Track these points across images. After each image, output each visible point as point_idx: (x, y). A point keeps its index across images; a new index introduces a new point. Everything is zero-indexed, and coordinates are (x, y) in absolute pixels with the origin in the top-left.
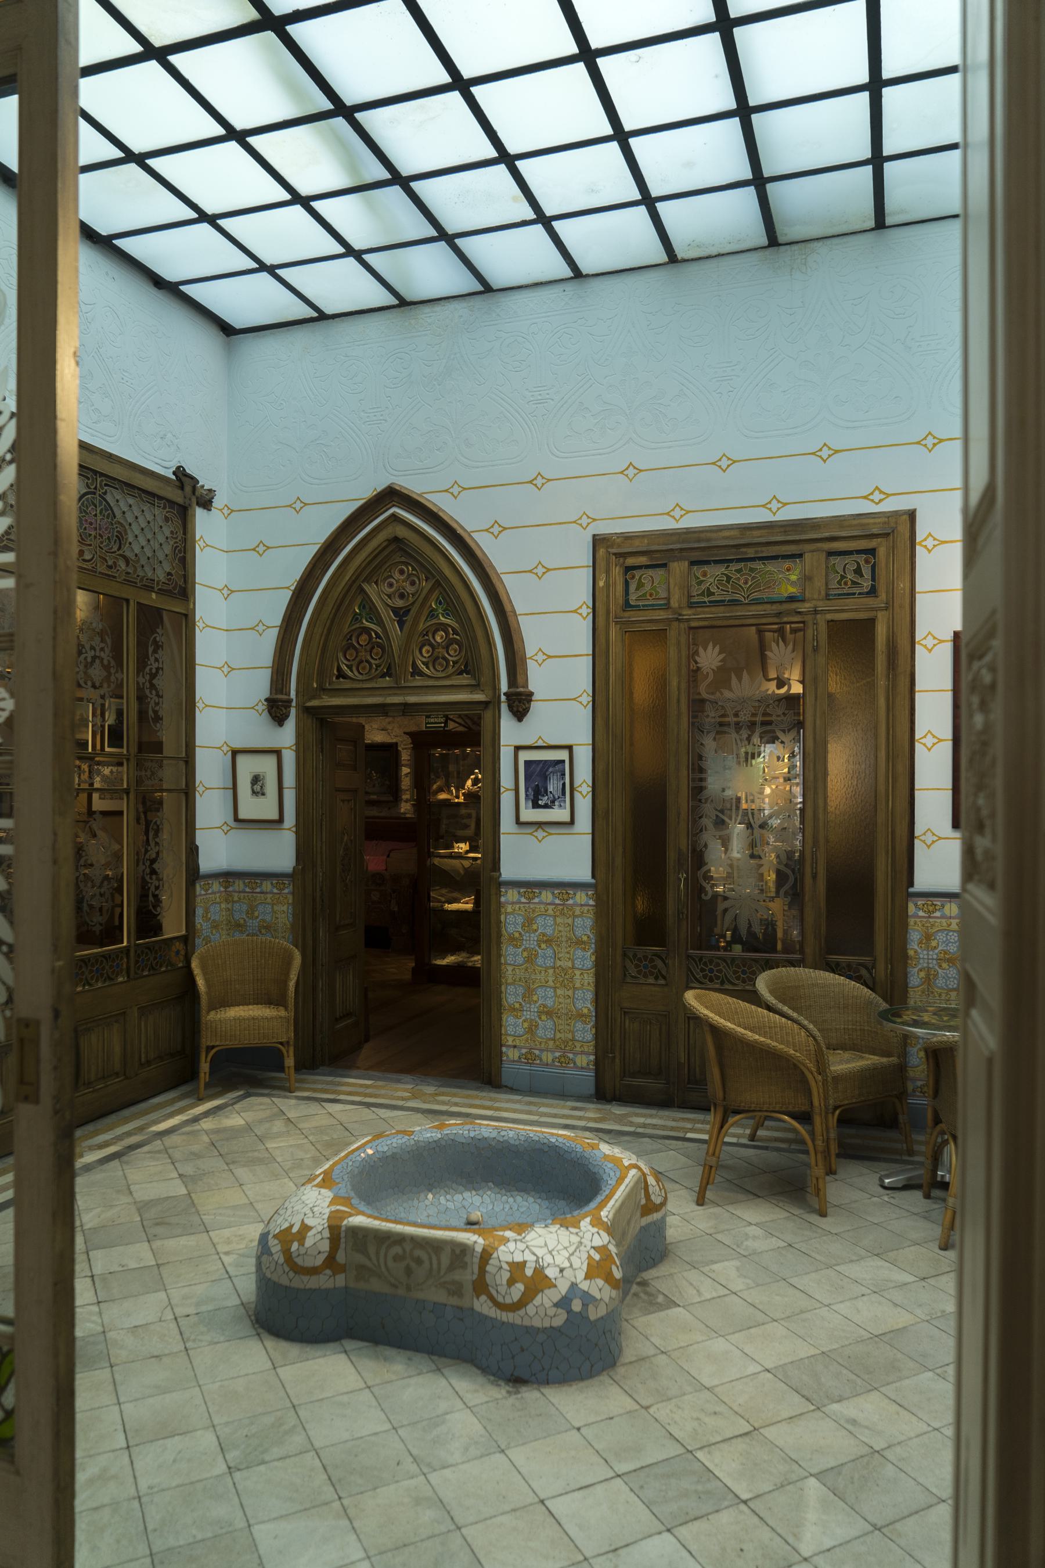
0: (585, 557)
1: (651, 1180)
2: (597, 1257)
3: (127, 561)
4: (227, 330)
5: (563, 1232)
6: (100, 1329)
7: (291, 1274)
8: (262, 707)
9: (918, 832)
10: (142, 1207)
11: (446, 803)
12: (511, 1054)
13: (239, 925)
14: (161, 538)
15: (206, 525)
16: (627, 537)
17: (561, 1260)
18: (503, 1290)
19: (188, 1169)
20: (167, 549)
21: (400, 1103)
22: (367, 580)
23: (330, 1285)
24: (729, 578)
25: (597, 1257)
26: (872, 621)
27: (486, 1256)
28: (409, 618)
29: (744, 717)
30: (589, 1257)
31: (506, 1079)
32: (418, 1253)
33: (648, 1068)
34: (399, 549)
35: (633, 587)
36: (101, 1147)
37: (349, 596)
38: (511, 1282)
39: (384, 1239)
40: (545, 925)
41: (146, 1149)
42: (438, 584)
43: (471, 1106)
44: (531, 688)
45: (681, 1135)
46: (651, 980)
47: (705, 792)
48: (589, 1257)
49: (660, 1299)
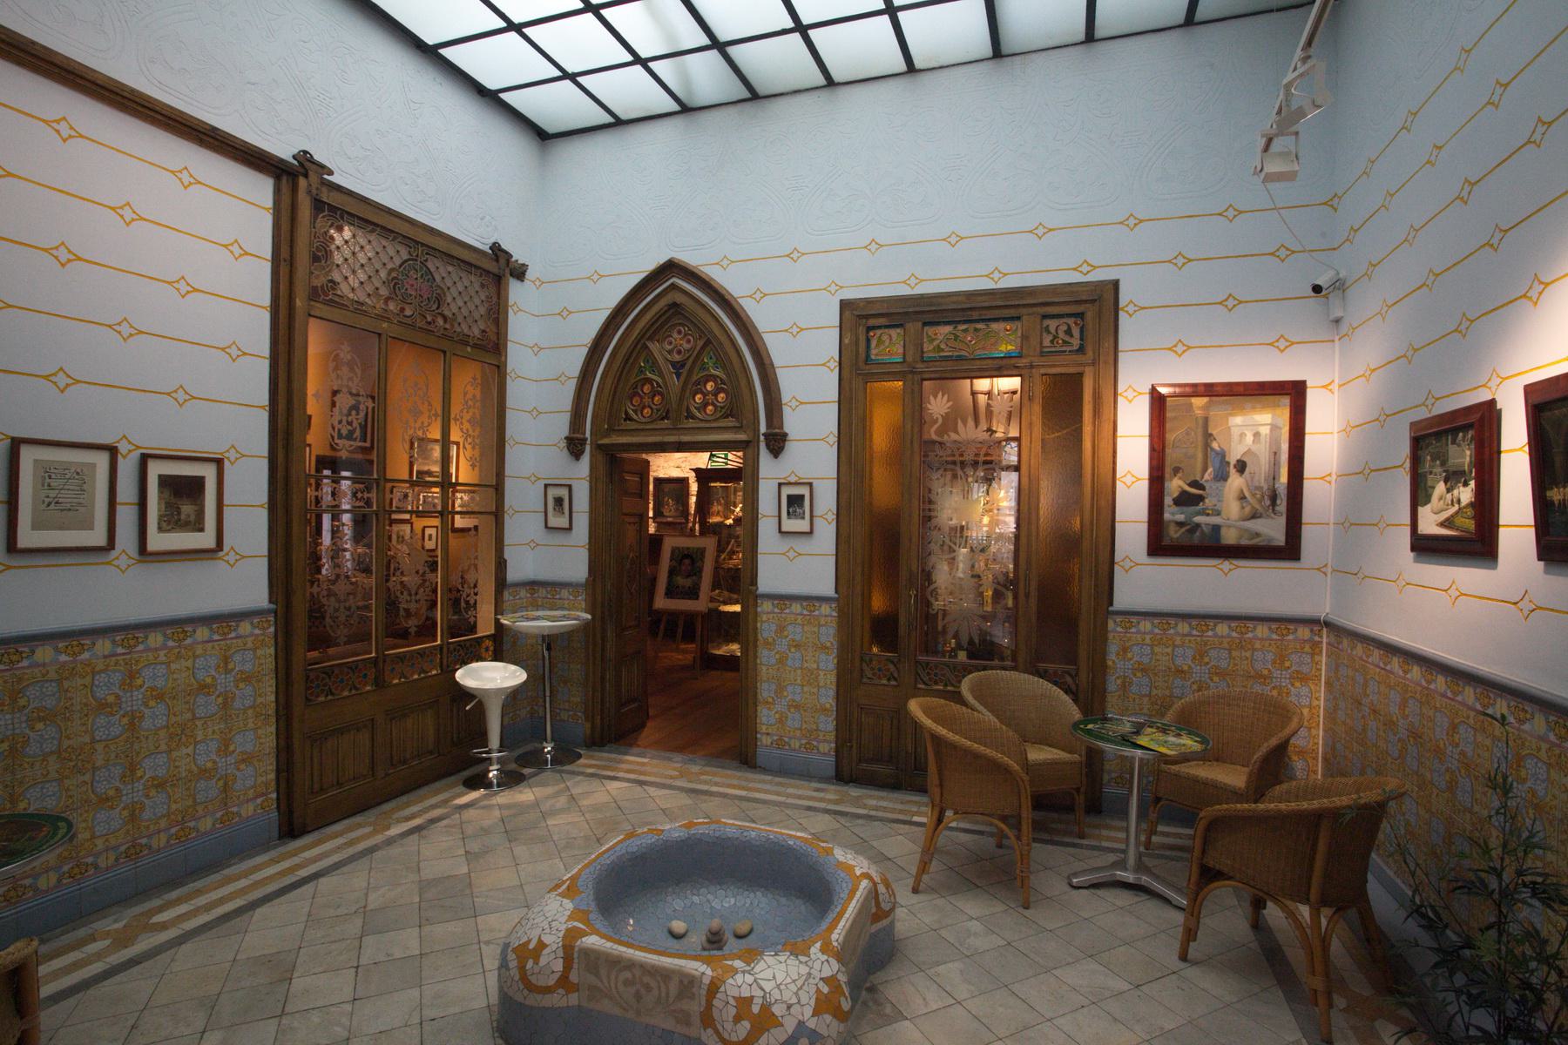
0: (835, 320)
1: (881, 889)
2: (825, 989)
3: (445, 319)
4: (542, 135)
5: (792, 961)
6: (346, 1034)
7: (526, 992)
8: (563, 444)
9: (1117, 558)
10: (424, 886)
11: (721, 524)
12: (765, 740)
13: (133, 770)
14: (477, 301)
15: (517, 292)
16: (869, 302)
17: (789, 996)
18: (729, 1026)
19: (474, 846)
20: (482, 310)
21: (668, 782)
22: (651, 339)
23: (563, 1003)
24: (956, 337)
25: (825, 989)
26: (1081, 375)
27: (714, 988)
28: (684, 371)
29: (969, 457)
30: (818, 991)
31: (760, 761)
32: (646, 979)
33: (876, 757)
34: (675, 314)
35: (874, 343)
36: (408, 819)
37: (636, 351)
38: (737, 1019)
39: (615, 963)
40: (794, 632)
41: (445, 822)
42: (708, 342)
43: (729, 786)
44: (786, 429)
45: (907, 818)
46: (884, 682)
47: (934, 522)
48: (818, 991)
49: (888, 1010)
